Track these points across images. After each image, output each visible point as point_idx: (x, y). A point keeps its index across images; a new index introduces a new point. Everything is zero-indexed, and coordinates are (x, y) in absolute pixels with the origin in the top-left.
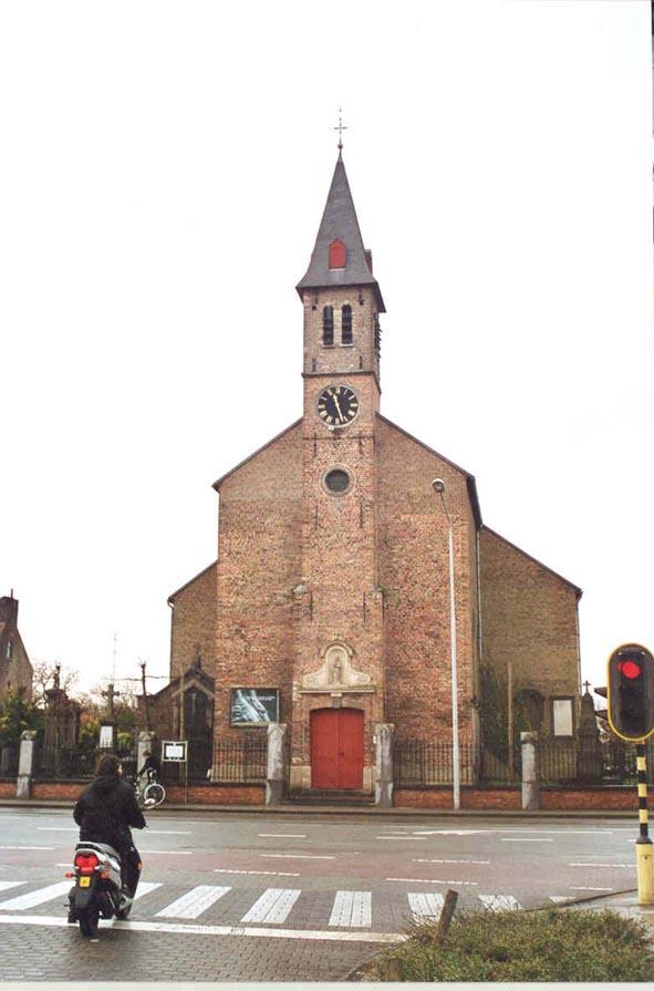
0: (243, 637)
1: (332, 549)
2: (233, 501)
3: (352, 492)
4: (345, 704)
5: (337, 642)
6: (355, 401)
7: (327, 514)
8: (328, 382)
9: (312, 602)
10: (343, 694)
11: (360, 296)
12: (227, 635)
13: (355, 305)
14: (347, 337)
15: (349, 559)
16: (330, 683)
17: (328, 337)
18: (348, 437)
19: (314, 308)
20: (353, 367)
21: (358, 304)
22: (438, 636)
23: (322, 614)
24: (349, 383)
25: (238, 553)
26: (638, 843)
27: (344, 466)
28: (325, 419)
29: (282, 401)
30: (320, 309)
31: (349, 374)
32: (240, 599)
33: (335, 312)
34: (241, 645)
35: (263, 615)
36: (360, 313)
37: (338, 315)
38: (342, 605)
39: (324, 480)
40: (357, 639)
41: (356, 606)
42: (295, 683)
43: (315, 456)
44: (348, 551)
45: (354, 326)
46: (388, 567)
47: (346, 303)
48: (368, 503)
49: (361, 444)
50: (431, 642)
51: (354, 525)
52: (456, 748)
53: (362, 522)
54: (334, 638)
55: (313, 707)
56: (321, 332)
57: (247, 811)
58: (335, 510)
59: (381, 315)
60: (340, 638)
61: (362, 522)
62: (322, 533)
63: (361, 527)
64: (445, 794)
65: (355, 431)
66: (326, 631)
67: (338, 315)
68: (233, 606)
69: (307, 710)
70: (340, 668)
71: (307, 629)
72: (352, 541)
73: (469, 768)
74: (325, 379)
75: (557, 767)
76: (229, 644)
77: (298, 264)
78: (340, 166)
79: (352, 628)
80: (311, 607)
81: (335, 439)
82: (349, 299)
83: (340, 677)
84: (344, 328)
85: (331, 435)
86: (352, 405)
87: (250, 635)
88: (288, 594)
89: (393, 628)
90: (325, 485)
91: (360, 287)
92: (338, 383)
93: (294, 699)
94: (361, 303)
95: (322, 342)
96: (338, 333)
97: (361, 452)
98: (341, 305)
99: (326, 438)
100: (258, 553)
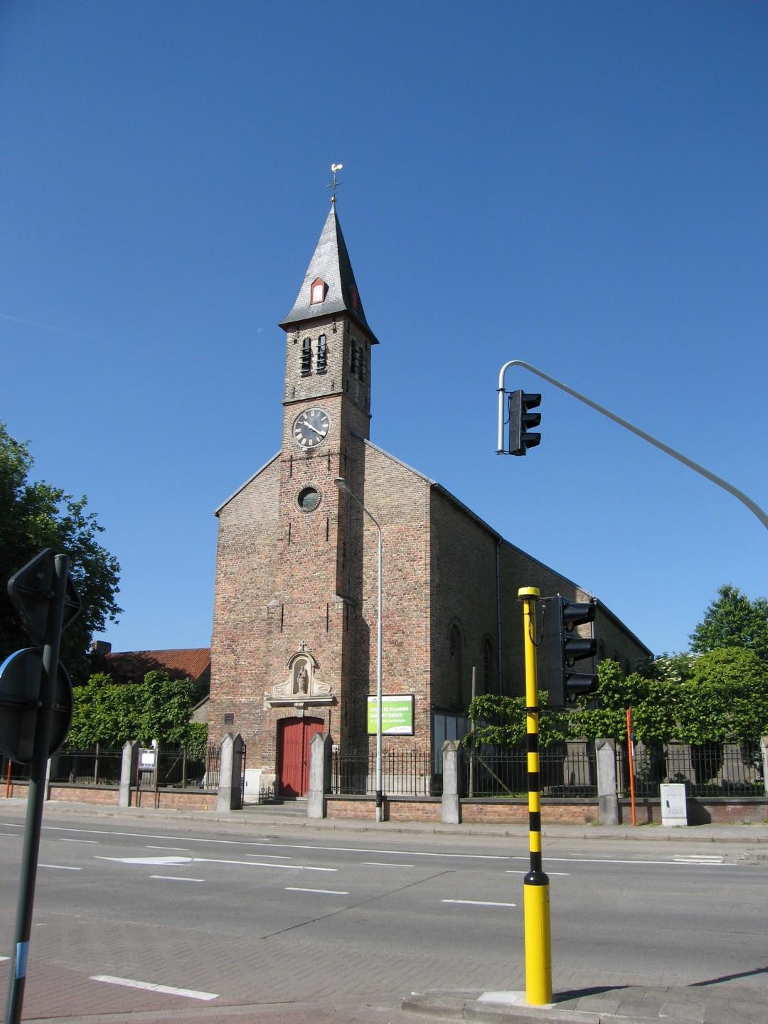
0: (233, 651)
2: (230, 526)
7: (298, 530)
12: (220, 650)
16: (295, 693)
18: (319, 456)
22: (400, 645)
25: (232, 573)
26: (527, 882)
28: (300, 441)
31: (322, 397)
35: (250, 630)
38: (309, 617)
41: (320, 617)
49: (329, 461)
50: (395, 650)
59: (374, 347)
68: (226, 623)
69: (275, 720)
72: (318, 555)
76: (222, 659)
79: (316, 638)
83: (305, 689)
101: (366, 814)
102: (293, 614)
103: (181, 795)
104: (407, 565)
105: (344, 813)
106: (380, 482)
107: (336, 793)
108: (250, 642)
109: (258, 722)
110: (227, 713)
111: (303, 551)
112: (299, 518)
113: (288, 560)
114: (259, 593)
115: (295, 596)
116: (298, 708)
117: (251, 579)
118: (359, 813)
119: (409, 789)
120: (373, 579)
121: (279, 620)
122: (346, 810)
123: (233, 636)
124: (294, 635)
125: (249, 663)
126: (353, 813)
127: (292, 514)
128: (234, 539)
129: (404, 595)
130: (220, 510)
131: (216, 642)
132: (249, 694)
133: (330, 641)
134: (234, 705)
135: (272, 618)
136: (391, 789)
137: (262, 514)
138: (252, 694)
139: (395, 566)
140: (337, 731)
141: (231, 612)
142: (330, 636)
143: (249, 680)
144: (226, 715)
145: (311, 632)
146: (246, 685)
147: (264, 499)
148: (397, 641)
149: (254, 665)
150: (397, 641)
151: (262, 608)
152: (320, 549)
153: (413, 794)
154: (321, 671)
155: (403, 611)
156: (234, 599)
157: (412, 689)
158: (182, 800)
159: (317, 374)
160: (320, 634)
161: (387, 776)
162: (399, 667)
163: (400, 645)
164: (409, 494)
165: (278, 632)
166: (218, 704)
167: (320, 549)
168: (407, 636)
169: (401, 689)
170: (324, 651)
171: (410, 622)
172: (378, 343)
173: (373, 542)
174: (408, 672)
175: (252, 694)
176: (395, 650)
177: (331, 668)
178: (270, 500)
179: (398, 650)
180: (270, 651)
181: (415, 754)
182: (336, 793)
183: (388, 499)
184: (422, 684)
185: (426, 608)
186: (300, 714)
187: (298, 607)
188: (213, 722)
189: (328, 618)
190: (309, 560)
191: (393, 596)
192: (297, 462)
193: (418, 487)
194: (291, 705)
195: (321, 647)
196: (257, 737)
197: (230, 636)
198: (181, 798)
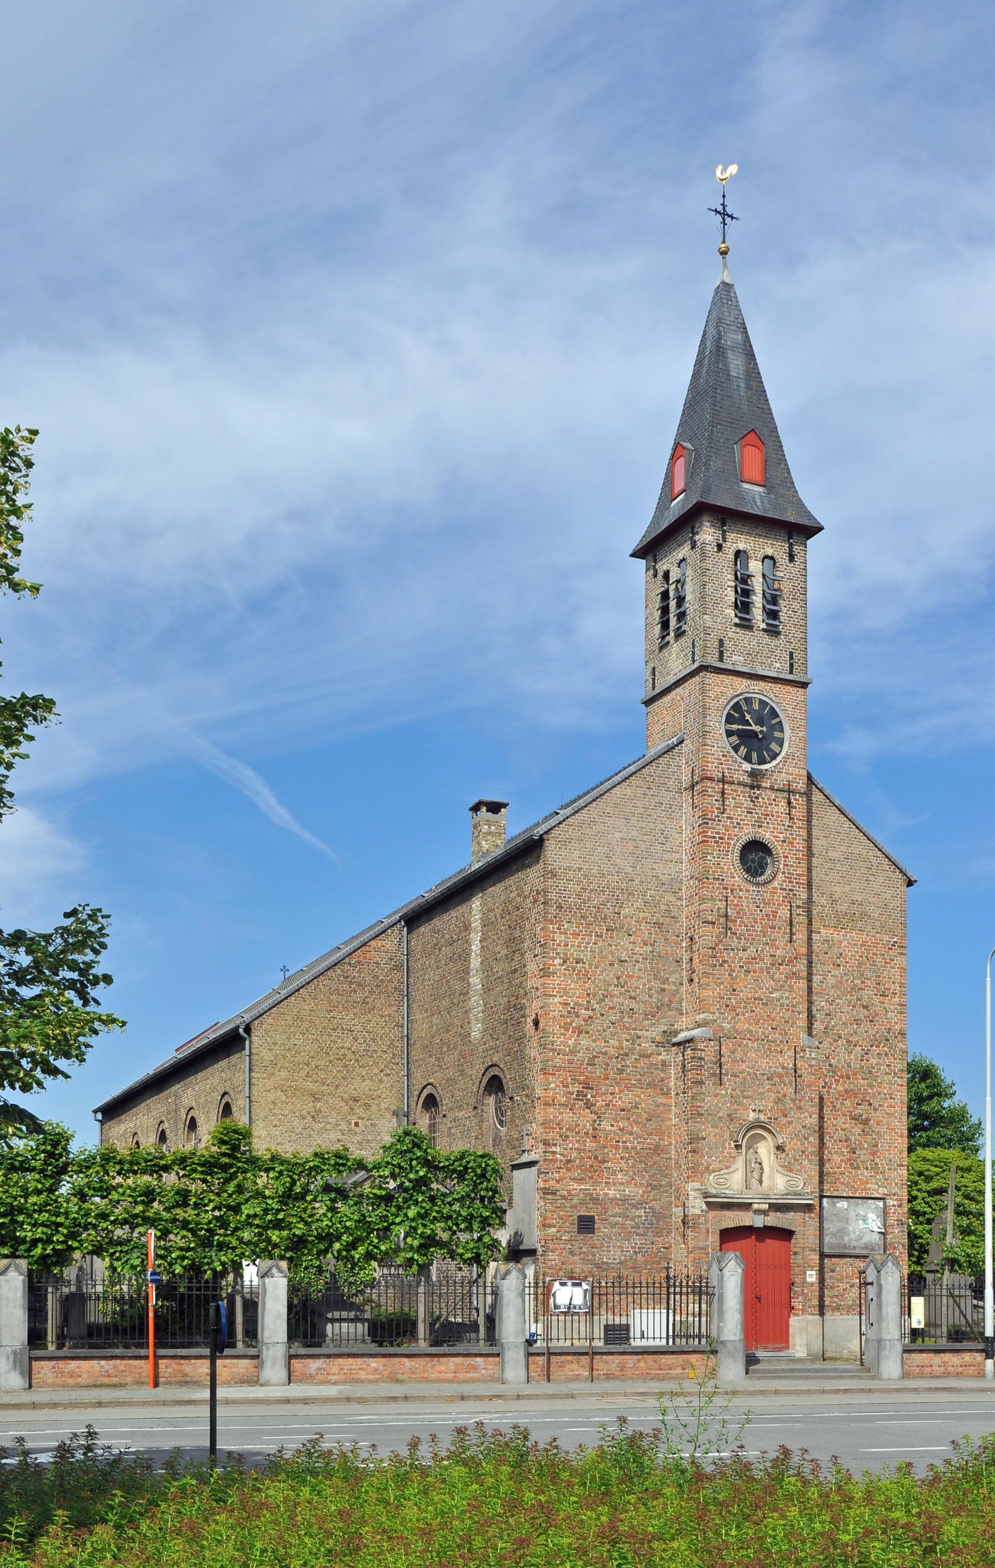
0: (589, 1105)
2: (570, 868)
8: (742, 685)
10: (771, 1205)
18: (772, 788)
19: (720, 547)
22: (866, 1122)
27: (766, 836)
32: (585, 1042)
34: (586, 1119)
35: (621, 1071)
38: (765, 1065)
39: (737, 854)
41: (783, 1068)
49: (789, 803)
50: (858, 1130)
51: (782, 940)
56: (731, 596)
60: (762, 1117)
62: (734, 942)
68: (572, 1052)
70: (760, 1164)
73: (330, 1335)
74: (737, 680)
79: (778, 1101)
81: (752, 787)
88: (658, 1039)
90: (737, 862)
92: (757, 690)
98: (760, 556)
99: (739, 784)
101: (961, 1369)
102: (738, 1055)
103: (640, 1357)
105: (930, 1369)
107: (700, 1343)
108: (621, 1091)
109: (641, 1231)
110: (582, 1213)
111: (751, 951)
112: (741, 890)
113: (724, 961)
114: (635, 1006)
115: (740, 1026)
116: (758, 1212)
117: (618, 978)
118: (951, 1369)
119: (657, 1335)
120: (826, 1015)
121: (715, 1063)
122: (931, 1366)
123: (587, 1078)
124: (742, 1092)
125: (621, 1130)
126: (942, 1368)
127: (729, 881)
128: (579, 896)
129: (872, 1046)
130: (546, 833)
131: (553, 1085)
132: (622, 1184)
133: (800, 1108)
134: (596, 1200)
135: (701, 1058)
136: (562, 1337)
137: (632, 860)
138: (628, 1183)
139: (858, 999)
140: (815, 1250)
141: (580, 1032)
142: (800, 1101)
143: (622, 1158)
144: (580, 1217)
145: (769, 1091)
146: (616, 1167)
147: (635, 833)
148: (861, 1116)
149: (631, 1134)
150: (861, 1116)
151: (640, 1033)
152: (778, 952)
153: (568, 1343)
154: (787, 1155)
155: (870, 1072)
156: (587, 1009)
158: (642, 1364)
159: (764, 630)
160: (784, 1096)
161: (644, 1311)
162: (863, 1155)
163: (866, 1122)
164: (877, 889)
165: (714, 1084)
166: (563, 1197)
167: (778, 952)
168: (876, 1110)
169: (866, 1189)
170: (790, 1123)
171: (880, 1090)
172: (631, 556)
173: (826, 953)
174: (877, 1164)
175: (628, 1183)
176: (858, 1130)
177: (803, 1152)
178: (645, 838)
179: (863, 1131)
180: (702, 1115)
181: (447, 1282)
182: (700, 1343)
183: (847, 888)
184: (896, 1184)
185: (902, 1071)
186: (759, 1222)
187: (747, 1046)
188: (554, 1230)
189: (795, 1072)
190: (761, 968)
191: (855, 1046)
192: (733, 787)
193: (890, 879)
194: (746, 1206)
195: (785, 1116)
196: (640, 1256)
197: (582, 1078)
198: (639, 1361)
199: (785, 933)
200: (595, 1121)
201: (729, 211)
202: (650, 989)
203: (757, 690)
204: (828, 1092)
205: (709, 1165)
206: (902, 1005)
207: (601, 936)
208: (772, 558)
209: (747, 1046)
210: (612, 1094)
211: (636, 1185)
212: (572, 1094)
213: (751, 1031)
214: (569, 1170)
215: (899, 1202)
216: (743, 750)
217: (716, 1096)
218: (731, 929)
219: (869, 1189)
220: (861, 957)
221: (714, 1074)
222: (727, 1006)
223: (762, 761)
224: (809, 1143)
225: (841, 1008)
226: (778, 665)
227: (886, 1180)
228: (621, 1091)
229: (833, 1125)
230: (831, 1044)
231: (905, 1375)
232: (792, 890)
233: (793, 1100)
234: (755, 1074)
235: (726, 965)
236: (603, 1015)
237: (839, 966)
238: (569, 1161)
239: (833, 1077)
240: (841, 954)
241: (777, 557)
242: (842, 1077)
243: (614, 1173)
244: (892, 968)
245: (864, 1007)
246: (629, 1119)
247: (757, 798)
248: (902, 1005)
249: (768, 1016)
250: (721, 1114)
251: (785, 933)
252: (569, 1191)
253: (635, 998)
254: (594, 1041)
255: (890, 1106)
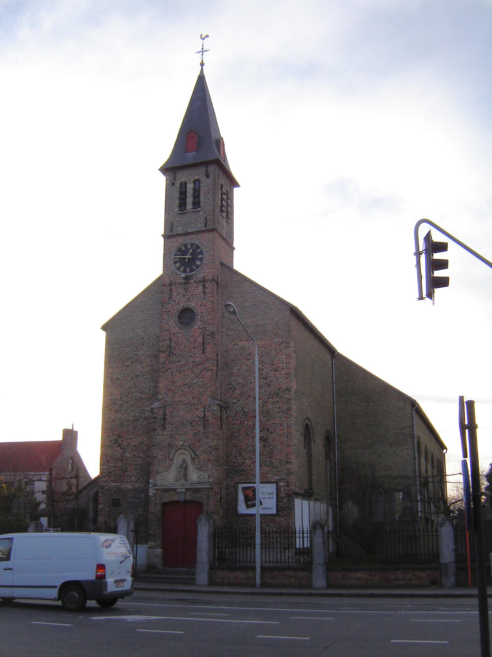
0: (119, 445)
1: (181, 372)
3: (198, 324)
4: (188, 497)
5: (182, 447)
6: (201, 253)
9: (165, 415)
11: (207, 171)
13: (203, 178)
14: (196, 204)
15: (194, 378)
17: (182, 205)
20: (200, 226)
21: (205, 177)
23: (173, 424)
24: (195, 239)
27: (192, 305)
29: (143, 263)
30: (178, 185)
31: (197, 232)
33: (188, 186)
36: (206, 184)
37: (190, 186)
40: (199, 444)
42: (151, 481)
43: (170, 298)
44: (193, 372)
45: (202, 194)
46: (228, 385)
47: (196, 177)
48: (209, 333)
49: (204, 286)
52: (258, 534)
53: (204, 349)
54: (181, 443)
55: (164, 501)
57: (234, 593)
58: (184, 340)
61: (204, 349)
63: (203, 352)
64: (250, 574)
65: (200, 277)
66: (175, 438)
67: (190, 186)
71: (162, 437)
75: (230, 550)
77: (164, 151)
78: (201, 81)
80: (164, 419)
82: (198, 174)
83: (185, 476)
84: (185, 198)
85: (183, 281)
86: (199, 256)
87: (125, 444)
89: (232, 434)
91: (206, 164)
92: (188, 240)
93: (150, 494)
94: (208, 176)
95: (177, 209)
96: (190, 200)
97: (204, 293)
98: (192, 181)
100: (132, 378)
104: (271, 374)
106: (247, 304)
111: (183, 361)
112: (178, 333)
115: (176, 399)
121: (162, 419)
124: (176, 432)
132: (134, 482)
138: (137, 481)
141: (117, 411)
143: (134, 469)
144: (114, 499)
145: (190, 430)
149: (139, 457)
151: (144, 408)
152: (197, 360)
155: (268, 413)
157: (276, 477)
166: (107, 490)
168: (272, 433)
170: (202, 445)
173: (242, 354)
174: (273, 463)
175: (137, 481)
177: (209, 460)
183: (254, 319)
184: (285, 473)
187: (179, 408)
188: (102, 505)
195: (199, 442)
199: (201, 349)
200: (122, 452)
201: (204, 53)
202: (150, 387)
203: (188, 240)
204: (243, 426)
205: (158, 470)
206: (287, 374)
207: (128, 366)
208: (198, 180)
209: (179, 408)
210: (131, 439)
211: (140, 482)
212: (112, 441)
213: (182, 401)
214: (109, 477)
215: (287, 484)
216: (182, 268)
217: (163, 435)
218: (172, 353)
219: (268, 477)
220: (262, 352)
221: (162, 425)
222: (170, 390)
223: (192, 270)
224: (212, 455)
225: (251, 380)
226: (199, 225)
227: (279, 471)
228: (135, 437)
229: (246, 444)
230: (245, 401)
231: (329, 586)
232: (205, 328)
233: (204, 433)
234: (183, 422)
235: (170, 371)
236: (127, 402)
237: (249, 359)
238: (110, 472)
239: (246, 418)
240: (250, 353)
241: (200, 178)
242: (250, 417)
243: (130, 477)
244: (281, 355)
245: (264, 378)
246: (138, 450)
247: (188, 288)
248: (287, 374)
249: (191, 392)
250: (165, 444)
251: (201, 349)
252: (109, 487)
253: (142, 392)
254: (123, 415)
255: (281, 430)
